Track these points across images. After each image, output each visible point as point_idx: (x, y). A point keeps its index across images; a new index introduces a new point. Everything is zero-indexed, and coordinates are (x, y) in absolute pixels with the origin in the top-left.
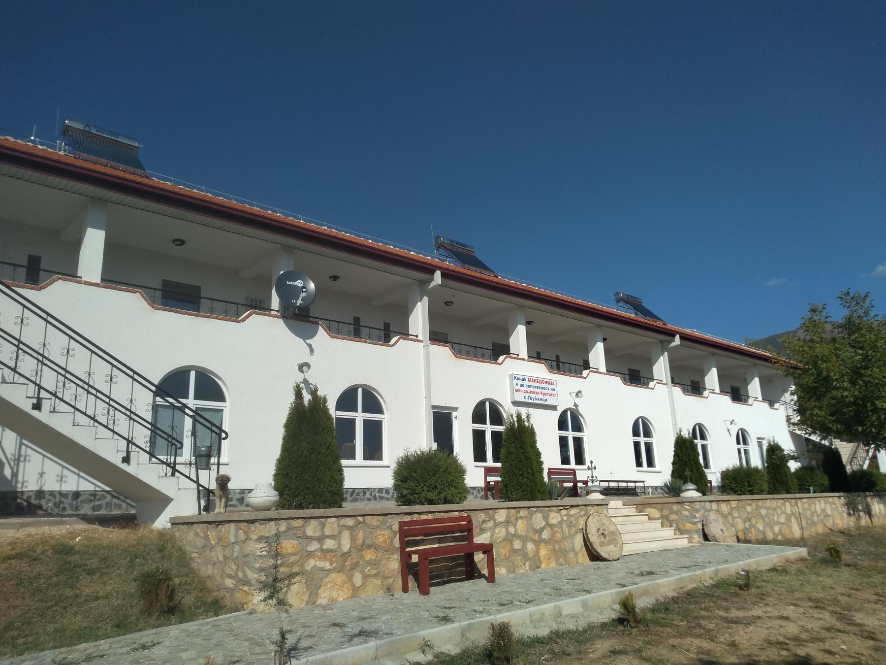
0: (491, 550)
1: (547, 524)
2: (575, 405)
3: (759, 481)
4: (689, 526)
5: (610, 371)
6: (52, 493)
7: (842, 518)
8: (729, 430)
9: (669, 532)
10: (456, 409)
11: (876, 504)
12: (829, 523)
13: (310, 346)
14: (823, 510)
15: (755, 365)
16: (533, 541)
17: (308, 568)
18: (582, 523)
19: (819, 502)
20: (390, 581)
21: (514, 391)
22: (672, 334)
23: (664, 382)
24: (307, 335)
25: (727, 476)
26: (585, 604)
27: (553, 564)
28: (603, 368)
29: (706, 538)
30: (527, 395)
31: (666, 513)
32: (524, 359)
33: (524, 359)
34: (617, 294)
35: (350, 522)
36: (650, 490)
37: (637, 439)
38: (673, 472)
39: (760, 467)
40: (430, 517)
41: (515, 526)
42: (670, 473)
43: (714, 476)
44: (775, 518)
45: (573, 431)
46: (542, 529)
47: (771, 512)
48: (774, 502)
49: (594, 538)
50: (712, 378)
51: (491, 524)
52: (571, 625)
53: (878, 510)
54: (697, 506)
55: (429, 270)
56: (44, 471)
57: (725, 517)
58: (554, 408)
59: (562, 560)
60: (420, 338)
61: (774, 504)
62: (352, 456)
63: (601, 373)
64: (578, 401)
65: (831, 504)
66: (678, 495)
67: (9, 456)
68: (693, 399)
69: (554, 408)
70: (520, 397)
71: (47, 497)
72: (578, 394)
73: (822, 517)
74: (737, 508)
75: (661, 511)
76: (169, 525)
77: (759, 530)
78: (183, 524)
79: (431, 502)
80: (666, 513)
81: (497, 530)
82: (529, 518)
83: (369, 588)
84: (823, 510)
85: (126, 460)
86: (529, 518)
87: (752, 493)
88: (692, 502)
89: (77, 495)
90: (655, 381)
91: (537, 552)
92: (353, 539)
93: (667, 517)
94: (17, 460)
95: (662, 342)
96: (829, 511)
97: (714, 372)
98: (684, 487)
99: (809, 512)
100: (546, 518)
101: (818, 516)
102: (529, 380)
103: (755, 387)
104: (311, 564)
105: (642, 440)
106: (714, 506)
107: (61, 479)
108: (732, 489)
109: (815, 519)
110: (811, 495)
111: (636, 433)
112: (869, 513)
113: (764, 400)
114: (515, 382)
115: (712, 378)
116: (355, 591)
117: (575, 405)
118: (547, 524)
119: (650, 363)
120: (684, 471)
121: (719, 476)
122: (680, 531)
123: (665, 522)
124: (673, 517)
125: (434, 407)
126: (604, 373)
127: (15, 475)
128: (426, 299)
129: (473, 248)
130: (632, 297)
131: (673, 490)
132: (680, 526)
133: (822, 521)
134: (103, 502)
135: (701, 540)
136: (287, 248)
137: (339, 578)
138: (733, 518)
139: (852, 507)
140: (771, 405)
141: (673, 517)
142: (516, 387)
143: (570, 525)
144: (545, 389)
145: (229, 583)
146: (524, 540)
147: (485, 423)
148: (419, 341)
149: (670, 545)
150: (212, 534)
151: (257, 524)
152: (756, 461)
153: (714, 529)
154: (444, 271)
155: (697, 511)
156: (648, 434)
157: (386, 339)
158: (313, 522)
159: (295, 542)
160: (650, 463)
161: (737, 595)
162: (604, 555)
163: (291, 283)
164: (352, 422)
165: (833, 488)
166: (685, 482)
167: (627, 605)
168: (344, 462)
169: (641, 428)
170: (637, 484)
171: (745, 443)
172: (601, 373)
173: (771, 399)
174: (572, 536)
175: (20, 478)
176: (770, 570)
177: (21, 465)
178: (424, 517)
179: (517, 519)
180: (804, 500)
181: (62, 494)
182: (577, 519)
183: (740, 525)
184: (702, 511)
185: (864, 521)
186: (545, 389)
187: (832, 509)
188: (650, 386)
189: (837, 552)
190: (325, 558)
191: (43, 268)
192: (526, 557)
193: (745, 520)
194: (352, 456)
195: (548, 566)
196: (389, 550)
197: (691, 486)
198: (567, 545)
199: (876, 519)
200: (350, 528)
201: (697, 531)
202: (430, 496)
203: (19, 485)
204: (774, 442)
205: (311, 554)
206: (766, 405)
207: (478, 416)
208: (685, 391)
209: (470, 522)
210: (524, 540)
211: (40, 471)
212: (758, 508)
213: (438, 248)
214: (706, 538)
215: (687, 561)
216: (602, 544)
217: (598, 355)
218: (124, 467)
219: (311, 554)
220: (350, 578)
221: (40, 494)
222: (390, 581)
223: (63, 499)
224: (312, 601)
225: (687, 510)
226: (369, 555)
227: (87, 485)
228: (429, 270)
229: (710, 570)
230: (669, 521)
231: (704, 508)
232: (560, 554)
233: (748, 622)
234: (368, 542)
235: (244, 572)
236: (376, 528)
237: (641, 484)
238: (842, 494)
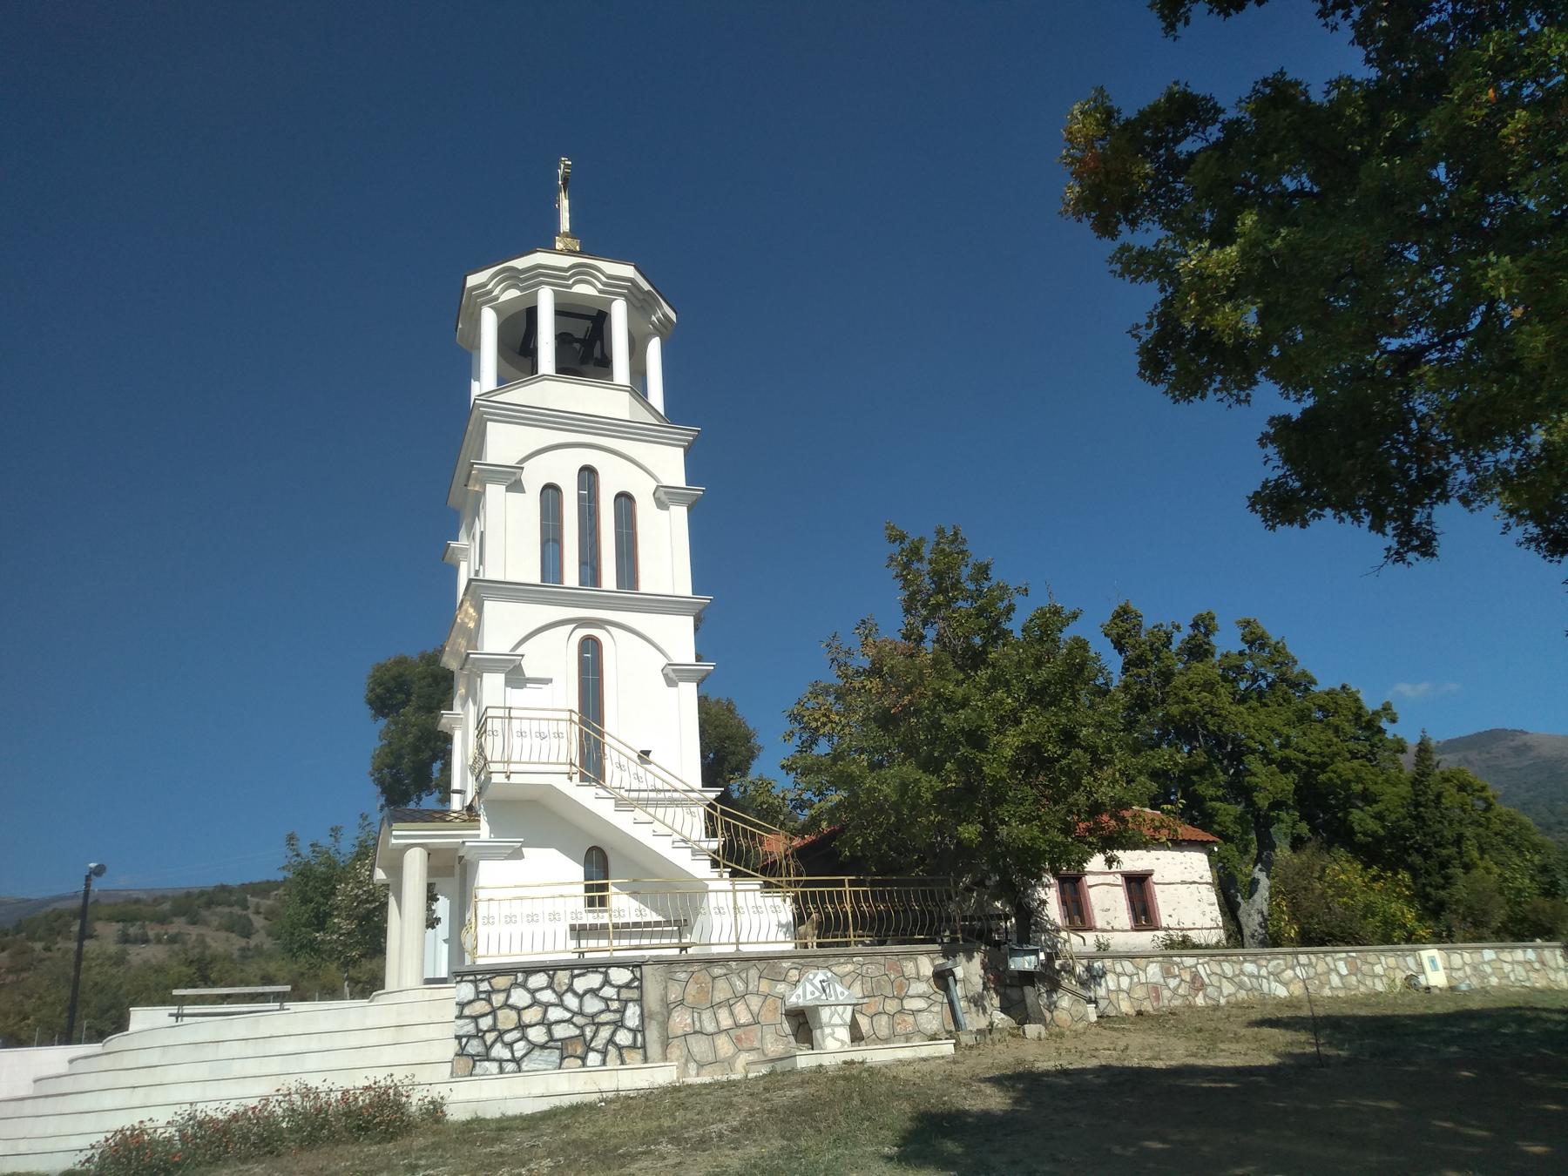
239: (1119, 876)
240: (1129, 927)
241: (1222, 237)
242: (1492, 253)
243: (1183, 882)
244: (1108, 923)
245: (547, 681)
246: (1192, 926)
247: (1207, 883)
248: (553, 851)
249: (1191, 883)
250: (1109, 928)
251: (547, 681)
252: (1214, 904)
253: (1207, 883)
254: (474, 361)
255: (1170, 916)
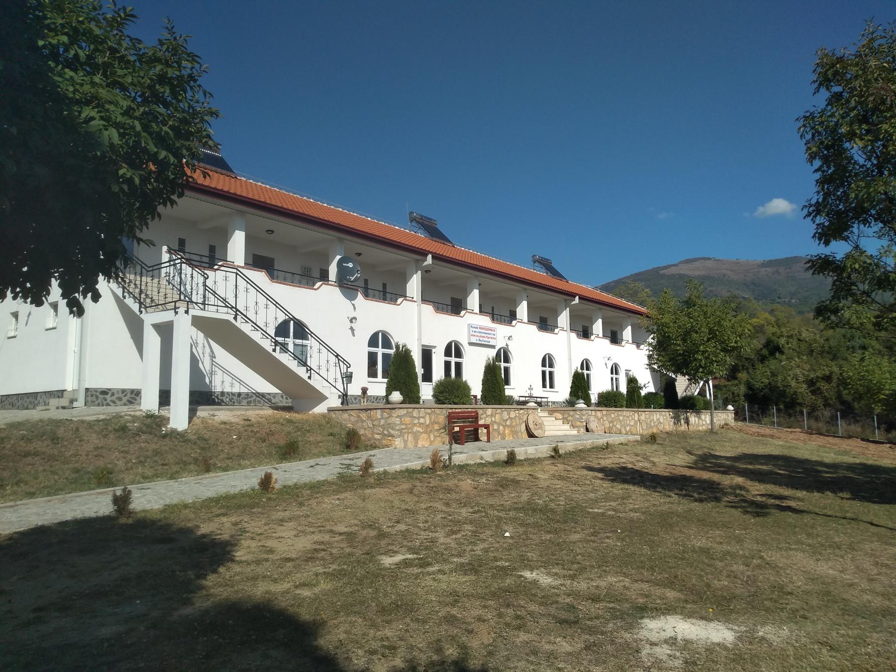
0: (489, 427)
1: (509, 417)
2: (507, 345)
3: (620, 400)
4: (578, 423)
5: (530, 321)
6: (228, 393)
7: (669, 425)
8: (606, 364)
9: (567, 427)
10: (435, 347)
11: (693, 418)
12: (661, 427)
13: (353, 305)
14: (658, 419)
15: (630, 317)
16: (503, 425)
17: (414, 430)
18: (525, 418)
19: (656, 414)
20: (444, 439)
21: (470, 335)
22: (573, 295)
23: (565, 329)
24: (351, 297)
25: (601, 396)
26: (536, 450)
27: (511, 438)
28: (525, 319)
29: (587, 430)
30: (478, 338)
31: (566, 416)
32: (477, 314)
33: (477, 314)
34: (534, 256)
35: (429, 411)
36: (550, 404)
37: (544, 369)
38: (571, 392)
40: (460, 410)
41: (495, 417)
42: (569, 393)
43: (594, 398)
44: (628, 422)
46: (507, 420)
47: (626, 418)
48: (628, 412)
49: (531, 426)
50: (598, 327)
51: (484, 416)
52: (532, 457)
53: (694, 422)
54: (584, 412)
55: (424, 254)
57: (599, 420)
58: (493, 347)
59: (515, 436)
60: (415, 299)
61: (628, 414)
63: (524, 323)
64: (509, 343)
65: (663, 416)
66: (574, 406)
67: (208, 371)
68: (584, 342)
69: (493, 347)
70: (473, 340)
71: (226, 395)
72: (510, 338)
73: (657, 423)
74: (606, 415)
75: (563, 415)
76: (326, 411)
77: (617, 428)
78: (338, 410)
79: (455, 404)
80: (566, 416)
81: (487, 419)
82: (501, 414)
83: (436, 442)
84: (658, 419)
85: (310, 378)
86: (501, 414)
87: (616, 406)
88: (581, 410)
89: (239, 394)
90: (559, 328)
91: (504, 431)
92: (430, 419)
93: (566, 418)
94: (211, 374)
95: (566, 300)
96: (661, 420)
97: (599, 322)
98: (577, 402)
99: (649, 420)
100: (509, 414)
101: (654, 423)
102: (480, 328)
103: (627, 333)
104: (415, 429)
105: (547, 369)
106: (593, 413)
107: (232, 385)
108: (604, 404)
109: (652, 424)
110: (652, 410)
111: (544, 365)
112: (687, 422)
113: (633, 342)
114: (472, 329)
115: (598, 327)
116: (431, 442)
117: (507, 345)
118: (509, 417)
119: (556, 314)
120: (578, 392)
121: (597, 396)
122: (573, 426)
123: (565, 420)
124: (570, 418)
125: (423, 346)
126: (526, 323)
127: (211, 382)
128: (419, 272)
129: (435, 221)
130: (544, 258)
131: (571, 403)
132: (574, 423)
133: (657, 426)
134: (252, 399)
135: (585, 431)
136: (341, 240)
138: (604, 420)
139: (677, 419)
140: (638, 347)
141: (570, 418)
142: (472, 333)
143: (520, 419)
144: (489, 334)
145: (377, 436)
146: (499, 424)
147: (451, 357)
148: (415, 301)
149: (568, 433)
150: (363, 415)
151: (397, 410)
152: (623, 389)
153: (593, 426)
155: (584, 415)
156: (551, 366)
157: (393, 301)
158: (416, 410)
159: (409, 419)
160: (552, 386)
161: (602, 451)
162: (537, 435)
163: (345, 265)
165: (667, 406)
166: (578, 399)
167: (556, 450)
168: (506, 387)
169: (548, 361)
170: (543, 400)
171: (617, 373)
172: (524, 323)
173: (637, 342)
174: (520, 425)
175: (213, 385)
176: (619, 444)
177: (213, 376)
178: (457, 410)
179: (496, 414)
180: (646, 413)
181: (233, 394)
182: (523, 416)
183: (607, 425)
184: (587, 416)
185: (683, 427)
186: (489, 334)
187: (664, 419)
188: (555, 332)
189: (655, 437)
190: (420, 427)
192: (499, 434)
193: (610, 423)
195: (509, 438)
197: (582, 401)
198: (518, 428)
199: (692, 427)
200: (429, 414)
201: (583, 426)
202: (456, 401)
203: (213, 388)
206: (634, 346)
207: (448, 353)
208: (578, 336)
209: (477, 414)
210: (499, 424)
212: (619, 415)
213: (411, 221)
214: (587, 430)
215: (577, 438)
216: (535, 429)
217: (522, 310)
218: (308, 381)
221: (223, 393)
222: (444, 439)
223: (233, 397)
224: (416, 446)
225: (578, 414)
227: (264, 386)
228: (424, 254)
229: (590, 442)
230: (567, 420)
231: (587, 413)
232: (514, 433)
233: (605, 459)
234: (436, 421)
235: (388, 431)
236: (438, 414)
237: (546, 400)
238: (671, 410)
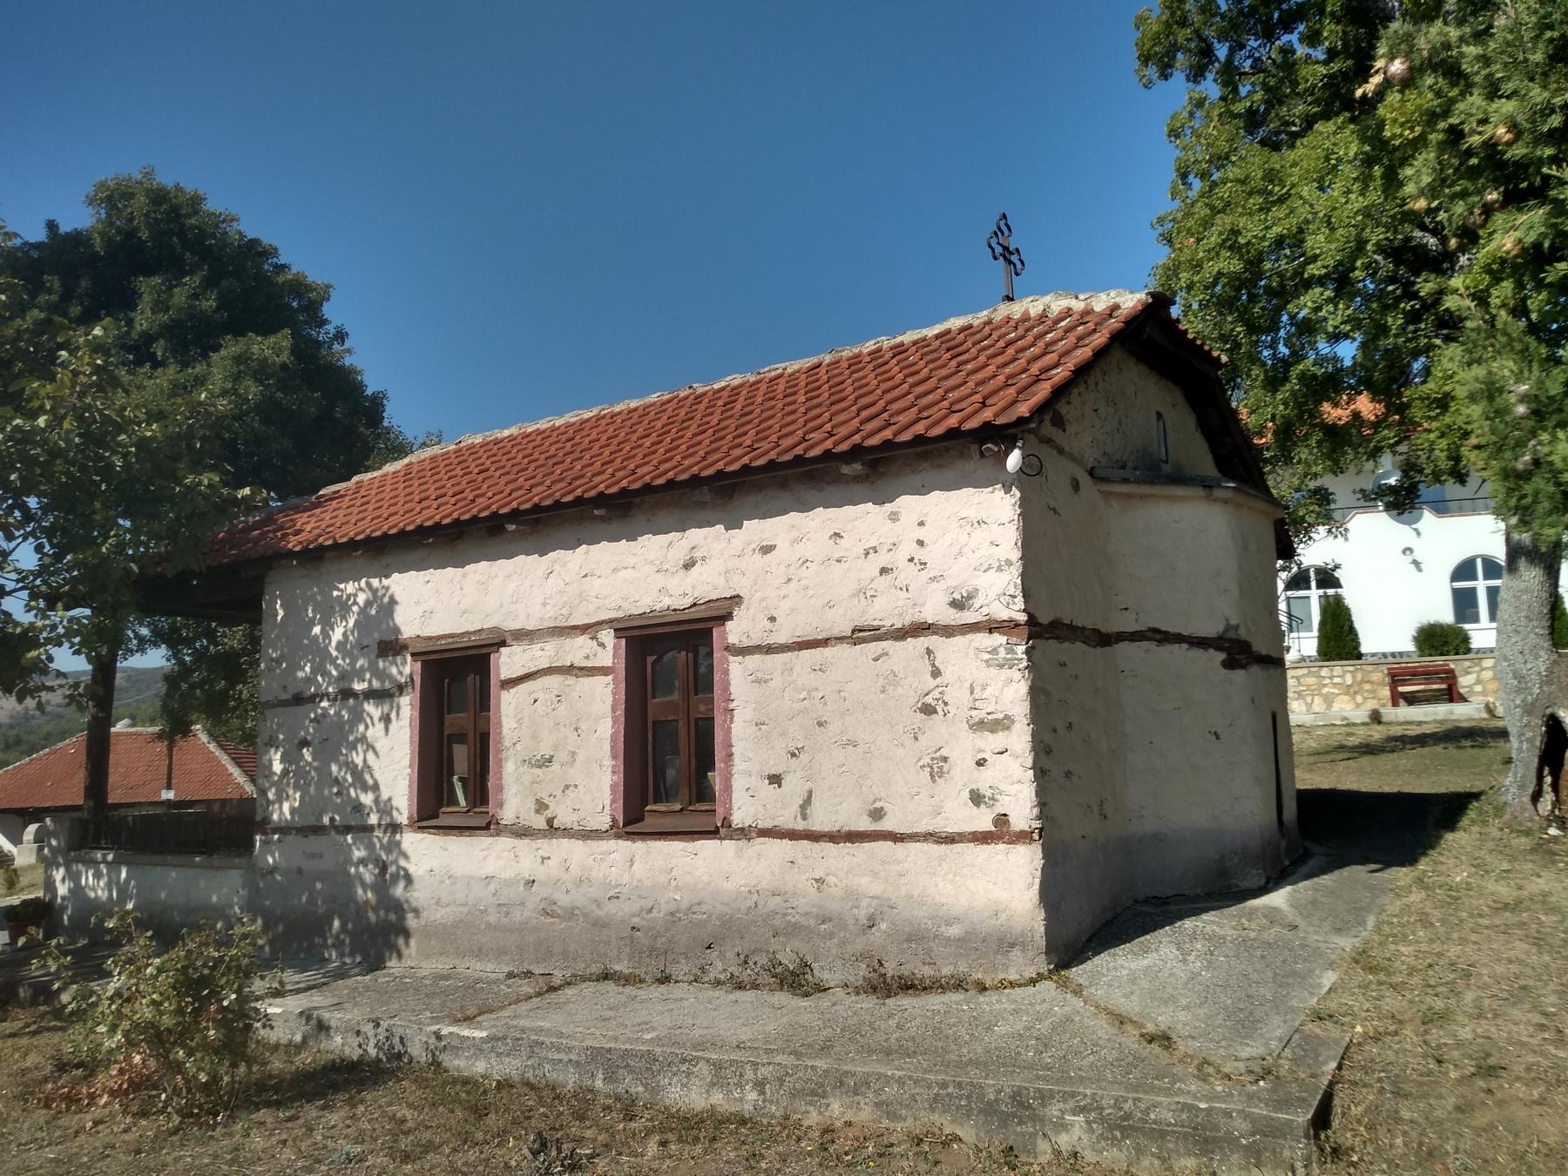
39: (1523, 559)
45: (1318, 587)
56: (161, 747)
62: (1476, 619)
104: (1325, 690)
137: (1346, 698)
154: (629, 633)
164: (1473, 591)
191: (79, 779)
194: (1476, 619)
196: (1382, 684)
204: (1482, 383)
205: (1325, 685)
211: (181, 743)
219: (1325, 685)
220: (1354, 699)
226: (1367, 687)
239: (608, 636)
240: (603, 822)
241: (218, 951)
242: (300, 674)
243: (861, 635)
244: (541, 806)
245: (810, 793)
246: (865, 824)
247: (992, 627)
248: (937, 492)
249: (901, 634)
250: (539, 822)
251: (810, 793)
252: (999, 725)
253: (992, 627)
254: (417, 739)
255: (775, 779)
